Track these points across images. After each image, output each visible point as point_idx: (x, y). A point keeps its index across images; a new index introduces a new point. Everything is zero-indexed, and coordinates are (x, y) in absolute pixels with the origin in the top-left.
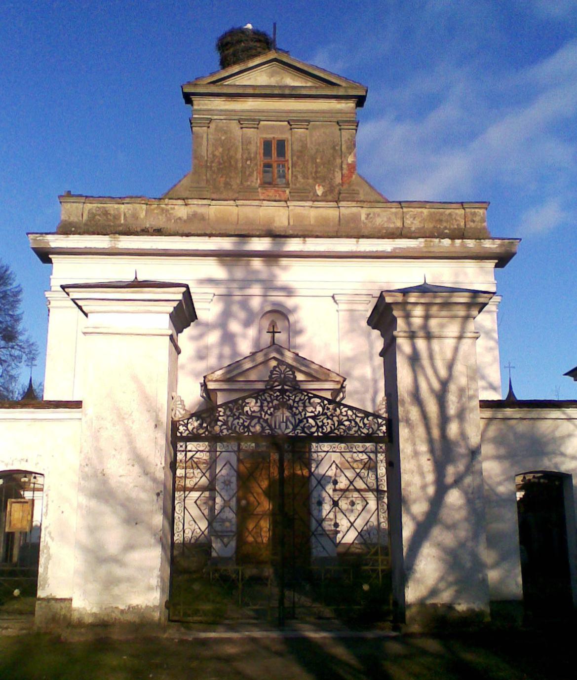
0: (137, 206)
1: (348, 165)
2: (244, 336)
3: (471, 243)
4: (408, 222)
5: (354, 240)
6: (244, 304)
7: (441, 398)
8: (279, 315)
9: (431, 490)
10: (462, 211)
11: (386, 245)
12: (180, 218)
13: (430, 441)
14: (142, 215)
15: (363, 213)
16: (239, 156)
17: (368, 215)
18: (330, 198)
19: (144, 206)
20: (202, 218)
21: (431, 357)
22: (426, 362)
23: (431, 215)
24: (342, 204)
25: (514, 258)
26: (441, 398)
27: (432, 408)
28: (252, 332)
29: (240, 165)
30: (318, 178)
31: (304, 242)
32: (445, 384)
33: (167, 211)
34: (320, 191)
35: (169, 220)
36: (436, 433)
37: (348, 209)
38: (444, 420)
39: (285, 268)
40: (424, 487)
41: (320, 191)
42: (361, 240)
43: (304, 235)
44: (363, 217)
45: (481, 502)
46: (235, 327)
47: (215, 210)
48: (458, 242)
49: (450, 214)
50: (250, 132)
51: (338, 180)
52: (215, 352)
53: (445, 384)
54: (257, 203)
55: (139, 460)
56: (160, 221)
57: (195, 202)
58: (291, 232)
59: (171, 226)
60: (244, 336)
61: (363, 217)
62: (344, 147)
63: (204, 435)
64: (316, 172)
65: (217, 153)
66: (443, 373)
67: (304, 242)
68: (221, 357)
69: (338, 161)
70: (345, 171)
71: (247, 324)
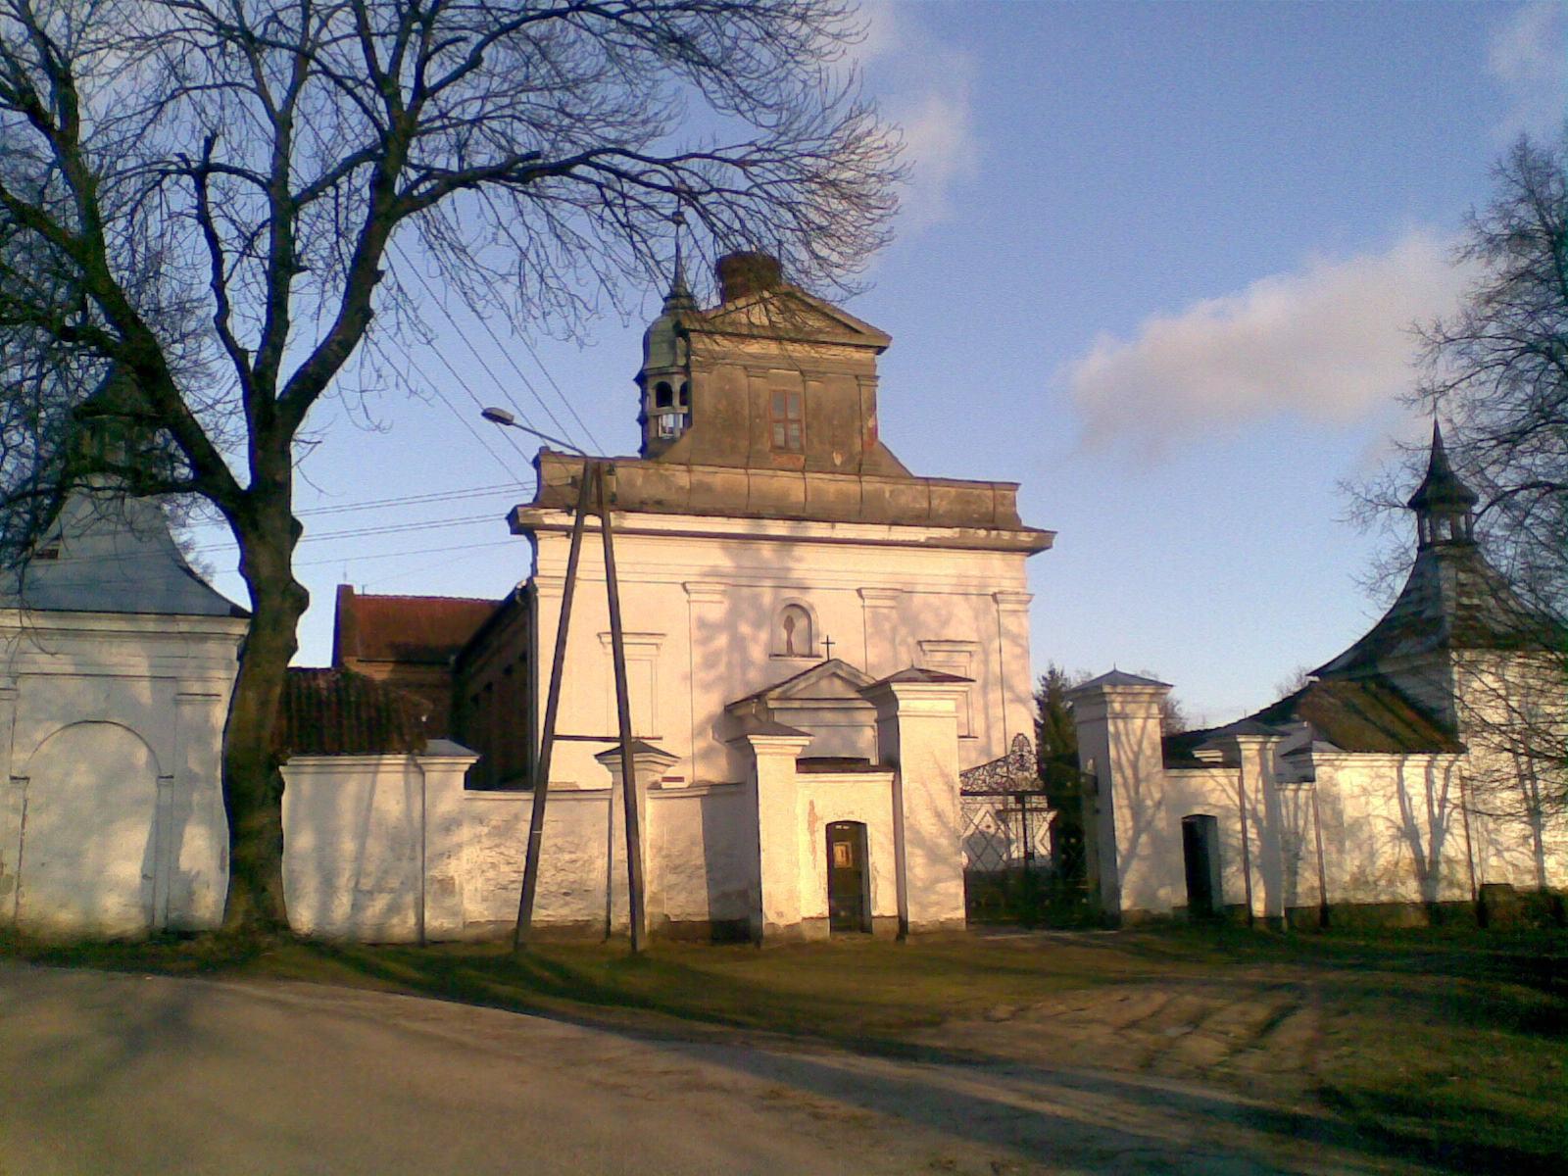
0: (633, 470)
1: (869, 429)
2: (755, 639)
3: (1006, 535)
4: (935, 502)
5: (886, 527)
6: (755, 601)
7: (1135, 767)
8: (796, 612)
9: (1130, 833)
10: (990, 493)
11: (920, 534)
12: (682, 488)
13: (1129, 797)
14: (639, 482)
15: (887, 488)
16: (746, 412)
17: (892, 492)
18: (849, 469)
19: (641, 472)
20: (708, 489)
21: (1127, 735)
22: (1123, 738)
23: (958, 495)
24: (864, 478)
25: (1042, 554)
26: (1135, 767)
27: (1129, 772)
28: (764, 636)
29: (747, 424)
30: (836, 444)
31: (833, 528)
32: (1137, 755)
33: (667, 477)
34: (838, 461)
35: (669, 489)
36: (1132, 794)
37: (871, 485)
38: (1137, 781)
39: (799, 560)
40: (1126, 831)
41: (838, 461)
42: (894, 528)
43: (831, 520)
44: (887, 495)
45: (1157, 840)
46: (745, 629)
47: (722, 478)
48: (994, 533)
49: (979, 496)
50: (757, 382)
51: (858, 447)
52: (724, 659)
53: (1137, 755)
54: (770, 472)
55: (939, 815)
56: (657, 491)
57: (701, 468)
58: (809, 511)
59: (671, 496)
60: (755, 639)
61: (887, 495)
62: (864, 407)
63: (1265, 823)
64: (834, 436)
65: (721, 407)
66: (1136, 748)
67: (833, 528)
68: (729, 664)
69: (857, 424)
70: (865, 437)
71: (757, 625)
